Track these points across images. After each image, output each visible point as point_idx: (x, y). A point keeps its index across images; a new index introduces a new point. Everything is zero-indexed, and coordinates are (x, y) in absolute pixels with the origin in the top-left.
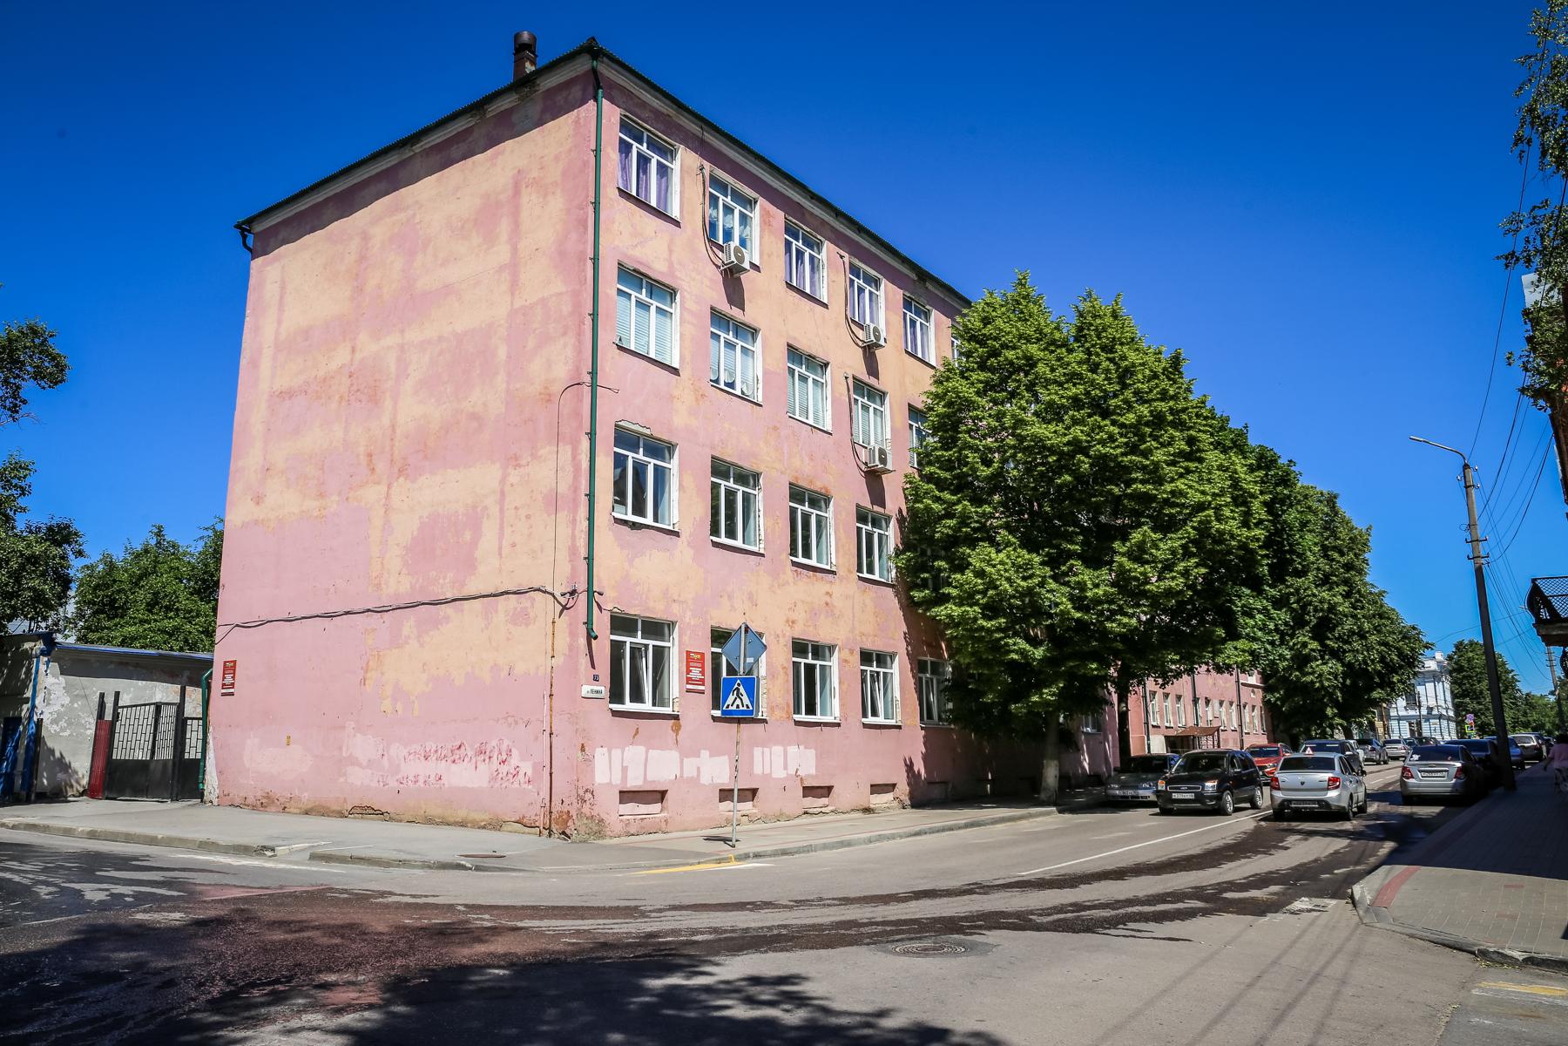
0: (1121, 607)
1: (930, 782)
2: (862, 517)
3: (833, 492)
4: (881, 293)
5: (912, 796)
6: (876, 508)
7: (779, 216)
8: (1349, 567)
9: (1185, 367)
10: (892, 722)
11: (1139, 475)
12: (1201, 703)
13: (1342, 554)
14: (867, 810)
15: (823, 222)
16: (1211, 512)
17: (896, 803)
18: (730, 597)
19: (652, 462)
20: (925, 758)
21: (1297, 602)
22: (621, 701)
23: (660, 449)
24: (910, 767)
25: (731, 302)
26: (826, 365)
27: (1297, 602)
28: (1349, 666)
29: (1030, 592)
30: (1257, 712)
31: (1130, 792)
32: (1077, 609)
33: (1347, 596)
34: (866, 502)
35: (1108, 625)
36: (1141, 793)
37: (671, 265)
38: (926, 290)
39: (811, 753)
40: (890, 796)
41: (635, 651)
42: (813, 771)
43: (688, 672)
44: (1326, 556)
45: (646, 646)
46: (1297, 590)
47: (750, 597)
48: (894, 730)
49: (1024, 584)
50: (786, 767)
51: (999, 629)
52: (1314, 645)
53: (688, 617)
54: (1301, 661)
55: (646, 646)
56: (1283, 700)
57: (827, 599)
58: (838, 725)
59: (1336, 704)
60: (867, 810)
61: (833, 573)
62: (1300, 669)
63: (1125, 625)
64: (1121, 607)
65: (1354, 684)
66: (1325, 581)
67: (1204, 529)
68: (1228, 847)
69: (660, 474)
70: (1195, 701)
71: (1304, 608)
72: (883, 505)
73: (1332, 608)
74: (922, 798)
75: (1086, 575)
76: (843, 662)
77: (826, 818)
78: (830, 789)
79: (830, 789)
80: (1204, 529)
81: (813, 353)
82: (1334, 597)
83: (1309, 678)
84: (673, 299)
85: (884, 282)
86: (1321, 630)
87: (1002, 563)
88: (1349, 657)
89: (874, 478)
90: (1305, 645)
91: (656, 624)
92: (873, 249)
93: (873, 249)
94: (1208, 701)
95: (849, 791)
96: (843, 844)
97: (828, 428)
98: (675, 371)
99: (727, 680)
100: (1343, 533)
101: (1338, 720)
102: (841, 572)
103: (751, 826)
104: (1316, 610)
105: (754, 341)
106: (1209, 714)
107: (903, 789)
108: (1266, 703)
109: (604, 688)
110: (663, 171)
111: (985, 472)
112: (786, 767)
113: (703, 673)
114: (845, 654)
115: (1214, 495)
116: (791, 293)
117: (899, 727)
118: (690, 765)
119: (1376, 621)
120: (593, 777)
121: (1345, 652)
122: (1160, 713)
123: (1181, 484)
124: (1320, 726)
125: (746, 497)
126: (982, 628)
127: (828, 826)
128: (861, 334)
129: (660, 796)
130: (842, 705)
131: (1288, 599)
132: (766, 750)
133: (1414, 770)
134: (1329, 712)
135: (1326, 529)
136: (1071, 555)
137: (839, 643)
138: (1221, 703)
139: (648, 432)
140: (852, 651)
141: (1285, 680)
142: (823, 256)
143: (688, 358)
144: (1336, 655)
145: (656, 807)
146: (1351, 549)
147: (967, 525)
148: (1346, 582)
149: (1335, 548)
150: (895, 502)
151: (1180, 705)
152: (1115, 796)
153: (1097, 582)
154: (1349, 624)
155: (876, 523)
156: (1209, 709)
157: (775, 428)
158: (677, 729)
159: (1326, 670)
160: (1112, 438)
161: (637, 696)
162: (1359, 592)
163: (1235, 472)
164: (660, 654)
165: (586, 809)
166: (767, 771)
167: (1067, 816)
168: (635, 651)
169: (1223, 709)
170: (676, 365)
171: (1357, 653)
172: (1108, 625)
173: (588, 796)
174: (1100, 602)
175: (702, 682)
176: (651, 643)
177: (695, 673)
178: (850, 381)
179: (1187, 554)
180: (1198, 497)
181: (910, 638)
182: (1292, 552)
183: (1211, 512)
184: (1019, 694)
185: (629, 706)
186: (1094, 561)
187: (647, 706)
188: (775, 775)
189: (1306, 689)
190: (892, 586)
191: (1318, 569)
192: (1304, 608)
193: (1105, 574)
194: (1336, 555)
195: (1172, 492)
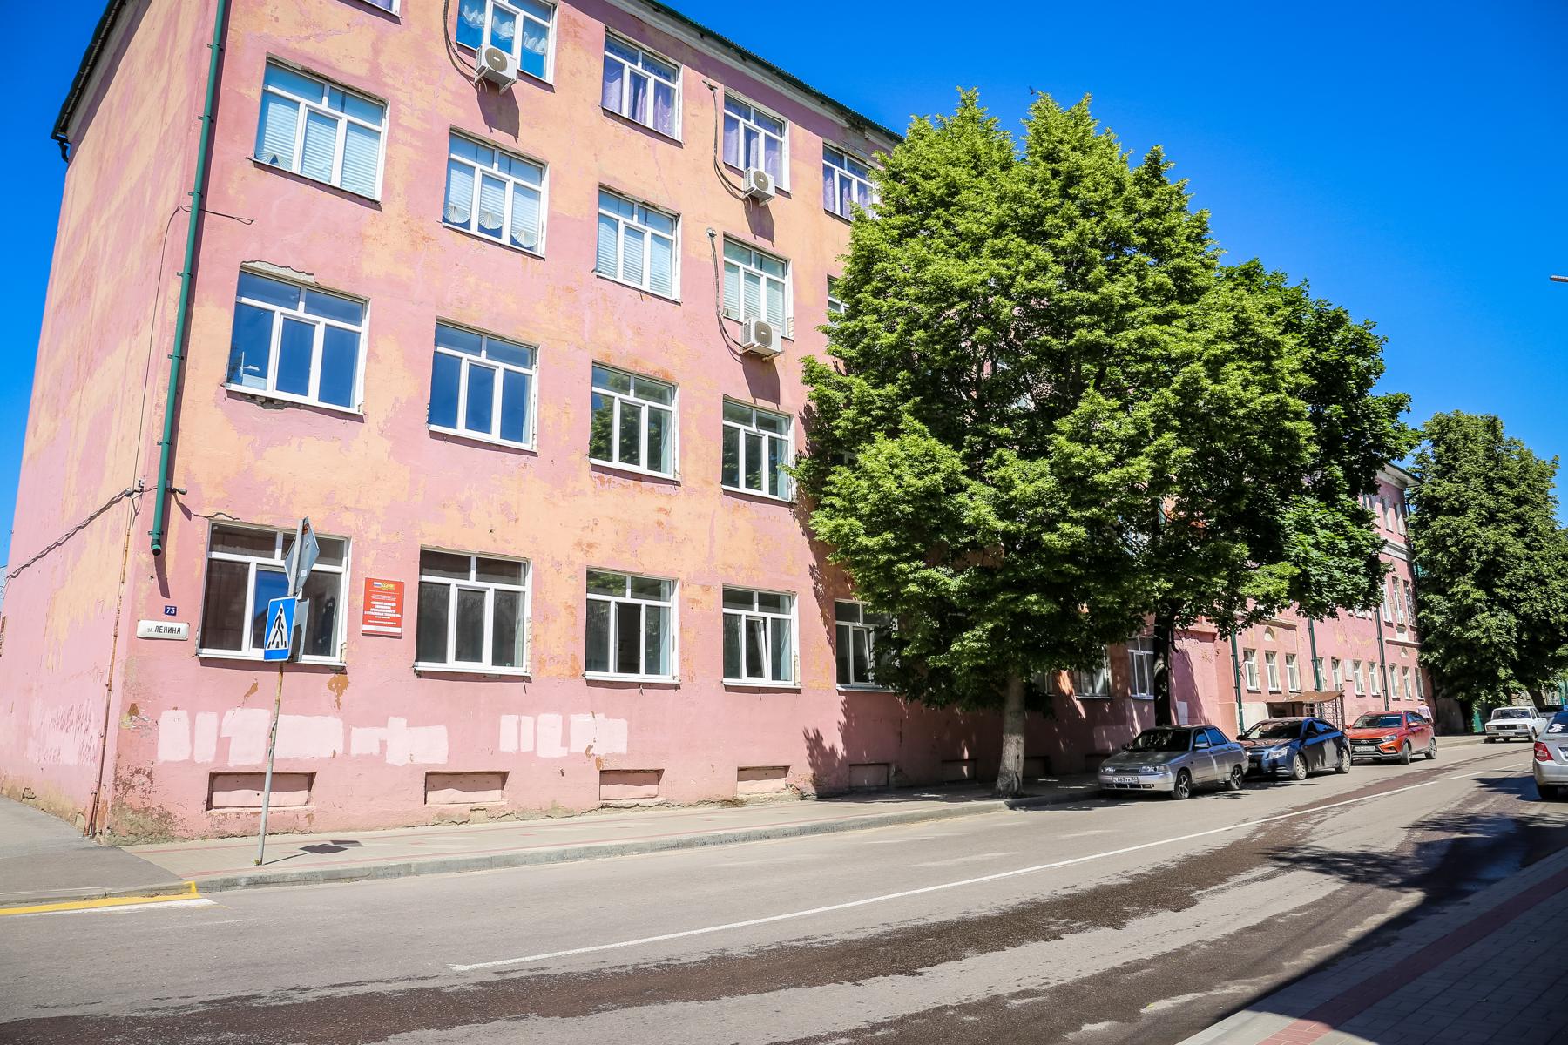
0: (1063, 510)
1: (852, 765)
2: (733, 410)
3: (677, 377)
4: (785, 140)
5: (817, 782)
6: (761, 403)
7: (596, 29)
8: (1520, 501)
9: (1168, 169)
10: (789, 685)
11: (1086, 319)
12: (1327, 663)
13: (1511, 485)
14: (733, 802)
15: (680, 44)
16: (1197, 366)
17: (789, 792)
18: (462, 508)
19: (766, 435)
20: (846, 731)
21: (1457, 544)
22: (737, 675)
23: (657, 389)
24: (815, 743)
25: (491, 121)
26: (677, 217)
27: (1457, 544)
28: (1526, 617)
29: (931, 493)
30: (1410, 674)
31: (1127, 779)
32: (1001, 518)
33: (1521, 534)
34: (743, 393)
35: (1046, 537)
36: (1143, 780)
37: (375, 68)
38: (854, 132)
39: (622, 724)
40: (780, 783)
41: (858, 634)
42: (622, 748)
43: (367, 606)
44: (1490, 489)
45: (638, 607)
46: (1455, 532)
47: (505, 508)
48: (812, 695)
49: (920, 483)
50: (566, 742)
51: (886, 548)
52: (1479, 594)
53: (374, 530)
54: (1464, 614)
55: (638, 607)
56: (1444, 661)
57: (662, 517)
58: (677, 687)
59: (1513, 664)
60: (733, 802)
61: (678, 483)
62: (1462, 622)
63: (1069, 536)
64: (1063, 510)
65: (1533, 640)
66: (1491, 519)
67: (1190, 391)
68: (985, 922)
69: (657, 419)
70: (1316, 661)
71: (1464, 551)
72: (775, 398)
73: (1500, 550)
74: (837, 783)
75: (1013, 466)
76: (688, 603)
77: (649, 812)
78: (659, 772)
79: (659, 772)
80: (1190, 391)
81: (651, 199)
82: (1503, 534)
83: (1473, 634)
84: (382, 114)
85: (789, 125)
86: (1489, 574)
87: (897, 461)
88: (1524, 608)
89: (758, 364)
90: (1466, 594)
91: (213, 532)
92: (769, 83)
93: (769, 83)
94: (1336, 662)
95: (682, 778)
96: (490, 863)
97: (676, 296)
98: (374, 204)
99: (622, 633)
100: (1513, 462)
101: (1514, 684)
102: (688, 483)
103: (492, 825)
104: (1480, 553)
105: (784, 274)
106: (1332, 678)
107: (803, 772)
108: (1423, 664)
109: (188, 626)
110: (664, 94)
111: (890, 338)
112: (566, 742)
113: (399, 608)
114: (694, 591)
115: (1209, 342)
116: (610, 121)
117: (798, 691)
118: (365, 740)
119: (1559, 564)
120: (153, 750)
121: (1519, 601)
122: (1233, 678)
123: (1153, 330)
124: (1492, 689)
125: (773, 442)
126: (866, 549)
127: (638, 822)
128: (742, 184)
129: (307, 780)
130: (683, 660)
131: (1444, 541)
132: (528, 721)
133: (1552, 748)
134: (1502, 673)
135: (1490, 458)
136: (1001, 442)
137: (682, 576)
138: (1357, 664)
139: (310, 280)
140: (706, 589)
141: (1444, 636)
142: (678, 86)
143: (399, 187)
144: (1506, 604)
145: (301, 795)
146: (1522, 479)
147: (868, 413)
148: (1517, 519)
149: (1502, 480)
150: (795, 397)
151: (1294, 665)
152: (1109, 784)
153: (1030, 478)
154: (1523, 569)
155: (770, 424)
156: (1339, 670)
157: (569, 290)
158: (340, 688)
159: (1493, 625)
160: (1043, 268)
161: (755, 670)
162: (1535, 530)
163: (1243, 310)
164: (778, 626)
165: (134, 798)
166: (527, 747)
167: (1019, 812)
168: (752, 626)
169: (1360, 671)
170: (377, 198)
171: (1535, 603)
172: (1046, 537)
173: (140, 779)
174: (1032, 505)
175: (398, 622)
176: (769, 616)
177: (383, 609)
178: (719, 241)
179: (1162, 425)
180: (1184, 347)
181: (820, 573)
182: (1379, 446)
183: (1197, 366)
184: (939, 643)
185: (746, 680)
186: (1033, 448)
187: (766, 680)
188: (542, 753)
189: (1471, 647)
190: (790, 505)
191: (1481, 505)
192: (1464, 551)
193: (1043, 465)
194: (1503, 488)
195: (1140, 340)
